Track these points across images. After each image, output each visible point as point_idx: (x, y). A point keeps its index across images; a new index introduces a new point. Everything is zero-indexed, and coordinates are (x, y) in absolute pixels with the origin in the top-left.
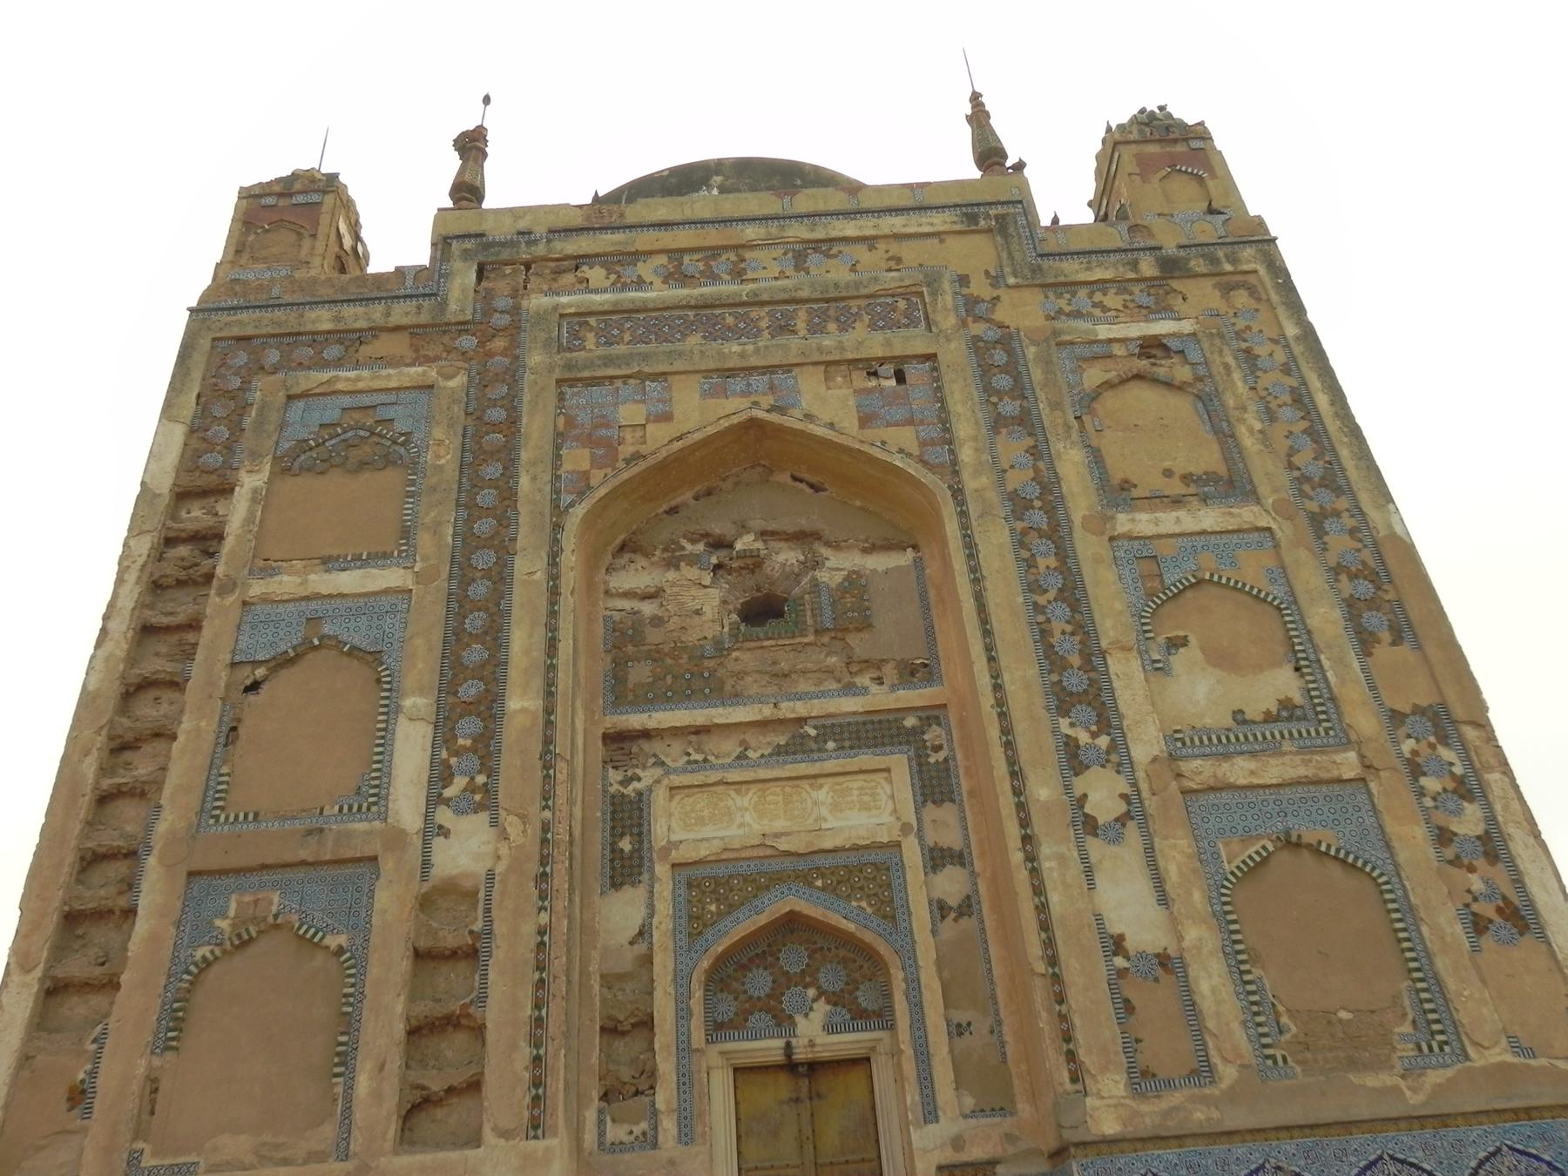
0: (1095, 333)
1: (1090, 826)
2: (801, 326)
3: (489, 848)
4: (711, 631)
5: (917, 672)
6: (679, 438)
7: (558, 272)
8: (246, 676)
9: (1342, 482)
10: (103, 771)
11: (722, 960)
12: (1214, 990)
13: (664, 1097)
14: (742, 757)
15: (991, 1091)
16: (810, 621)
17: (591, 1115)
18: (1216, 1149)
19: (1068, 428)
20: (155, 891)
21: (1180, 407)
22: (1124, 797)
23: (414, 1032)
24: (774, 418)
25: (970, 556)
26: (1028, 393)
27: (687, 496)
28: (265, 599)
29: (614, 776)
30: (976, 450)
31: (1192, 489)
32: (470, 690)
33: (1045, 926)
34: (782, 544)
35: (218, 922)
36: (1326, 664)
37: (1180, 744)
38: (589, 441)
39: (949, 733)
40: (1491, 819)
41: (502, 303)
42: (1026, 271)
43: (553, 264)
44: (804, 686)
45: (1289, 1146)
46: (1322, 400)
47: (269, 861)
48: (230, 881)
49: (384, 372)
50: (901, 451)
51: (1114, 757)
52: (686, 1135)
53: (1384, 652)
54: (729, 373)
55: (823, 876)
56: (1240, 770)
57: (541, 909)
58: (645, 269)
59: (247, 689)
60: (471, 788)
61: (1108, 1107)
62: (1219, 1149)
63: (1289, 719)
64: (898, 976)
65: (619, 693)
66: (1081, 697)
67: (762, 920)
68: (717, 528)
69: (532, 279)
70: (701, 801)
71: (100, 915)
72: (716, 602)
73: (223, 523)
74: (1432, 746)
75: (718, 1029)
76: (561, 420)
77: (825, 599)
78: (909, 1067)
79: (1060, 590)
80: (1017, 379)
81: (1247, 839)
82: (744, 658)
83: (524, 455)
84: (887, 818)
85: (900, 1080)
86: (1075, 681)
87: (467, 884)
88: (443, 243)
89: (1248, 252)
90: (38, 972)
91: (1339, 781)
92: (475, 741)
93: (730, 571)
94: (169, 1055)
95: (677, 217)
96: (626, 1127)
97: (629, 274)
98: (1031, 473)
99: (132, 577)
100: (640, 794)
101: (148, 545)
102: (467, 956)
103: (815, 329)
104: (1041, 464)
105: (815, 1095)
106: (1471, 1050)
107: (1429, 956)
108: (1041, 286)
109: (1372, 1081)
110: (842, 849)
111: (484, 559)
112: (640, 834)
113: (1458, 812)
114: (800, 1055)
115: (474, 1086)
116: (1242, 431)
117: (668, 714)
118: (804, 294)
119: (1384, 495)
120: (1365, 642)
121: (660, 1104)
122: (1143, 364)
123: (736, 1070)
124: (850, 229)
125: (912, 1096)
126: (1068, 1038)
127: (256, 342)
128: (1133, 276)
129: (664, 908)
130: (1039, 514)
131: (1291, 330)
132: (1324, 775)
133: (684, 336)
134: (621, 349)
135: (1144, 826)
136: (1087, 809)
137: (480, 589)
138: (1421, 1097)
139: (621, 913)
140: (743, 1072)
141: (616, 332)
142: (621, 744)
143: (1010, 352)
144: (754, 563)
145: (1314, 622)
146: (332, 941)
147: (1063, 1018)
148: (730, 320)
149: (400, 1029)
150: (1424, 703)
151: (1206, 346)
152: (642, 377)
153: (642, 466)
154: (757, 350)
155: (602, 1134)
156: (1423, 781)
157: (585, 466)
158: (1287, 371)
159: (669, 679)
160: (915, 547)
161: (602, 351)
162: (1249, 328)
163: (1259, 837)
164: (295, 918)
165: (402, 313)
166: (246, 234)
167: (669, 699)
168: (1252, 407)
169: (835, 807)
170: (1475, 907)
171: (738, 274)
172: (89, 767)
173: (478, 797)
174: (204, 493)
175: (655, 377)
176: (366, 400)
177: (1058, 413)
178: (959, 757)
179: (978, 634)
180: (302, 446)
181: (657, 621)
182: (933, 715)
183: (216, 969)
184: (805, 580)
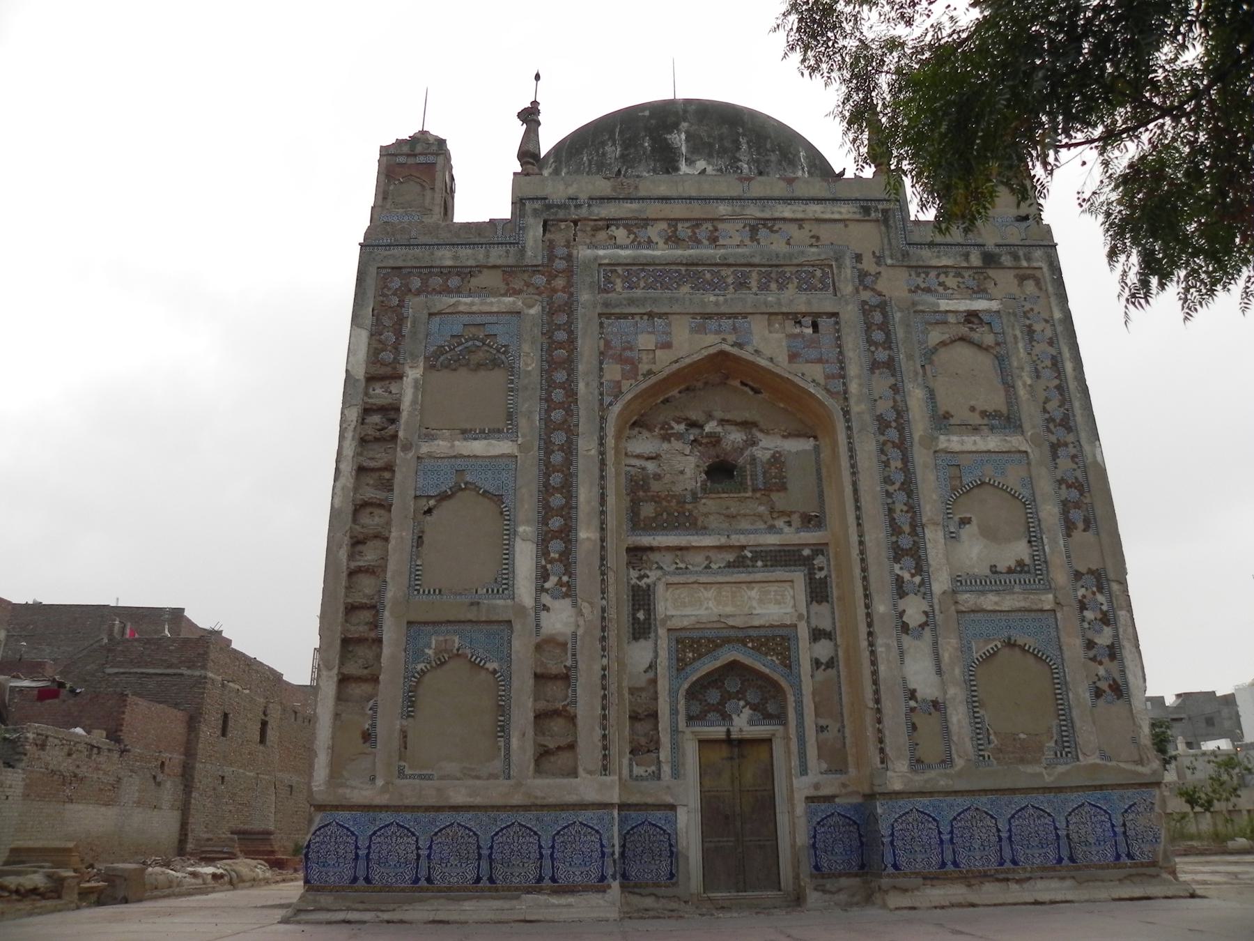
0: (938, 305)
1: (905, 628)
2: (754, 284)
3: (572, 620)
4: (690, 485)
5: (811, 521)
6: (676, 362)
7: (596, 229)
8: (424, 504)
9: (1072, 424)
10: (351, 557)
11: (694, 684)
12: (959, 721)
13: (664, 754)
14: (708, 567)
15: (836, 760)
16: (749, 483)
17: (625, 761)
18: (948, 799)
19: (916, 374)
20: (391, 632)
21: (984, 362)
22: (926, 613)
23: (537, 717)
24: (735, 351)
25: (851, 457)
26: (893, 346)
27: (675, 392)
28: (430, 456)
29: (634, 574)
30: (860, 385)
31: (986, 421)
32: (556, 523)
33: (875, 683)
34: (733, 428)
35: (427, 651)
36: (1045, 540)
37: (960, 582)
38: (621, 360)
39: (828, 560)
40: (1116, 636)
41: (561, 251)
42: (899, 255)
43: (592, 223)
44: (745, 525)
45: (984, 799)
46: (1069, 366)
47: (452, 619)
48: (430, 628)
49: (489, 300)
50: (814, 381)
51: (922, 589)
52: (676, 774)
53: (1078, 535)
54: (708, 316)
55: (752, 641)
56: (989, 601)
57: (603, 656)
58: (653, 232)
59: (425, 513)
60: (560, 583)
61: (898, 777)
62: (949, 799)
63: (1020, 572)
64: (791, 699)
65: (636, 523)
66: (906, 552)
67: (718, 664)
68: (693, 416)
69: (579, 234)
70: (683, 593)
71: (360, 641)
72: (693, 466)
73: (399, 400)
74: (1094, 593)
75: (690, 719)
76: (602, 342)
77: (759, 469)
78: (794, 747)
79: (902, 484)
80: (888, 334)
81: (988, 641)
82: (709, 504)
83: (581, 368)
84: (789, 610)
85: (788, 752)
86: (906, 542)
87: (561, 639)
88: (519, 202)
89: (1038, 253)
90: (335, 671)
91: (1042, 611)
92: (560, 555)
93: (701, 444)
94: (410, 720)
95: (674, 194)
96: (643, 768)
97: (642, 235)
98: (891, 403)
99: (349, 435)
100: (649, 586)
101: (356, 415)
102: (562, 678)
103: (764, 287)
104: (898, 398)
105: (742, 756)
106: (1081, 757)
107: (1070, 709)
108: (908, 267)
109: (1030, 769)
110: (764, 627)
111: (559, 438)
112: (649, 610)
113: (1100, 632)
114: (734, 736)
115: (572, 747)
116: (1019, 383)
117: (665, 538)
118: (756, 260)
119: (1095, 436)
120: (1069, 527)
121: (662, 757)
122: (964, 330)
123: (700, 741)
124: (787, 211)
125: (795, 762)
126: (881, 741)
127: (404, 271)
128: (965, 264)
129: (663, 655)
130: (893, 426)
131: (1057, 315)
132: (1035, 607)
133: (679, 285)
134: (638, 293)
135: (934, 630)
136: (905, 619)
137: (557, 458)
138: (1052, 779)
139: (640, 654)
140: (704, 743)
141: (635, 279)
142: (637, 554)
143: (885, 315)
144: (715, 440)
145: (1043, 515)
146: (491, 666)
147: (880, 731)
148: (708, 276)
149: (532, 715)
150: (1094, 568)
151: (1005, 321)
152: (651, 315)
153: (653, 380)
154: (726, 301)
155: (631, 771)
156: (1086, 613)
157: (618, 377)
158: (1051, 343)
159: (665, 515)
160: (815, 438)
161: (626, 294)
162: (1032, 310)
163: (994, 640)
164: (468, 651)
165: (497, 256)
166: (388, 184)
167: (665, 528)
168: (1027, 368)
169: (761, 601)
170: (1099, 684)
171: (714, 240)
172: (343, 554)
173: (564, 589)
174: (382, 378)
175: (660, 316)
176: (478, 320)
177: (911, 363)
178: (833, 576)
179: (853, 508)
180: (440, 351)
181: (657, 477)
182: (819, 549)
183: (428, 676)
184: (747, 453)
